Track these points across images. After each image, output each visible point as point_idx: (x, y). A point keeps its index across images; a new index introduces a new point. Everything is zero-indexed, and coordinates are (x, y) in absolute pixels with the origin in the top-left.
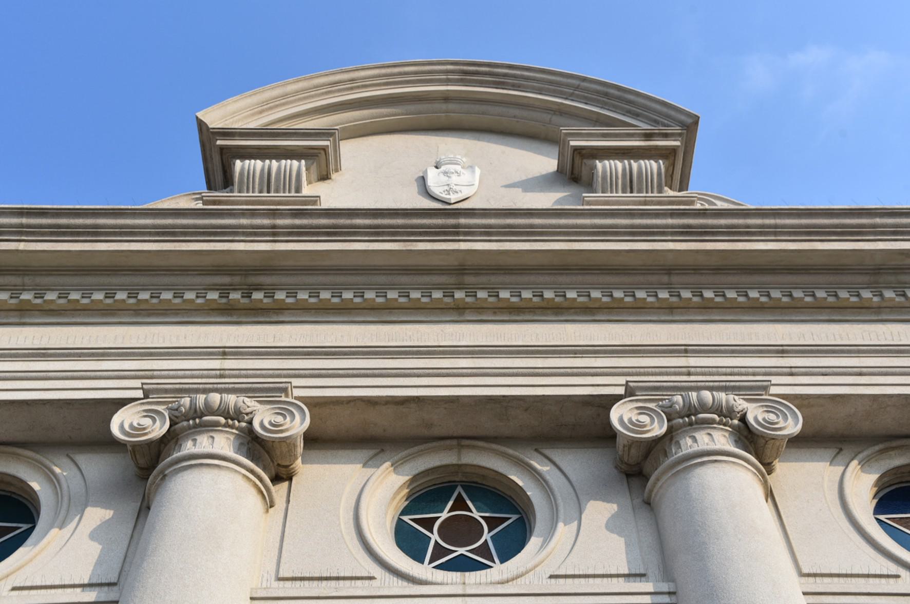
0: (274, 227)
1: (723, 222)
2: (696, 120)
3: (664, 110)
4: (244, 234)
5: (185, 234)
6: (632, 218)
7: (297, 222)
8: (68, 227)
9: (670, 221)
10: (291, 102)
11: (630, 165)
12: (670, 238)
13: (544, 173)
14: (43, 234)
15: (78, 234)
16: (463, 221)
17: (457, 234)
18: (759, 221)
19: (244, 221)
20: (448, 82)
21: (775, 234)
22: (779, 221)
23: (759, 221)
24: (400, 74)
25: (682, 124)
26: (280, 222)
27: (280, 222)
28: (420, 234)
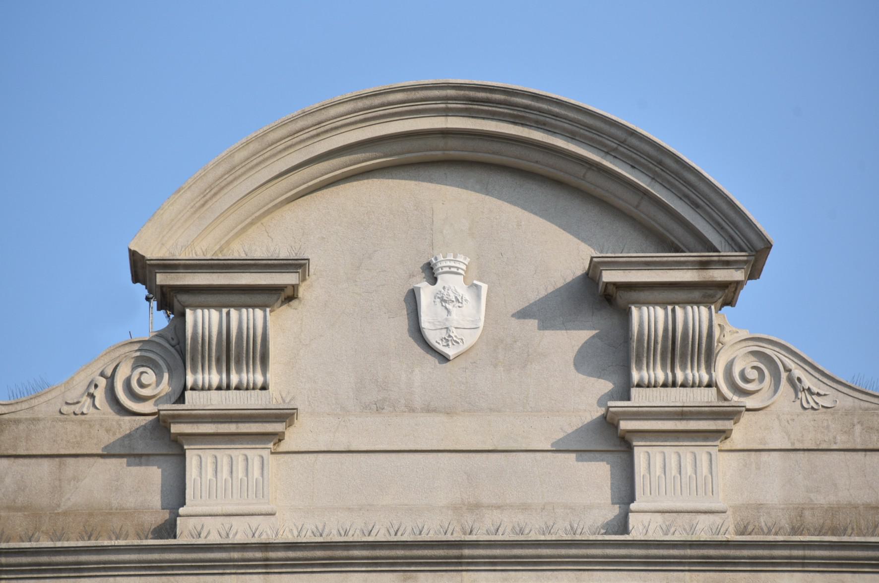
0: (267, 560)
1: (746, 552)
2: (768, 246)
3: (732, 214)
4: (234, 567)
5: (173, 568)
6: (647, 549)
7: (291, 554)
8: (49, 564)
9: (689, 552)
10: (240, 176)
11: (673, 311)
12: (687, 568)
13: (560, 284)
14: (23, 572)
15: (60, 571)
16: (466, 552)
17: (461, 564)
18: (786, 553)
19: (236, 555)
20: (446, 112)
21: (803, 565)
22: (808, 553)
23: (786, 553)
24: (383, 105)
25: (752, 248)
26: (272, 555)
27: (272, 555)
28: (421, 564)
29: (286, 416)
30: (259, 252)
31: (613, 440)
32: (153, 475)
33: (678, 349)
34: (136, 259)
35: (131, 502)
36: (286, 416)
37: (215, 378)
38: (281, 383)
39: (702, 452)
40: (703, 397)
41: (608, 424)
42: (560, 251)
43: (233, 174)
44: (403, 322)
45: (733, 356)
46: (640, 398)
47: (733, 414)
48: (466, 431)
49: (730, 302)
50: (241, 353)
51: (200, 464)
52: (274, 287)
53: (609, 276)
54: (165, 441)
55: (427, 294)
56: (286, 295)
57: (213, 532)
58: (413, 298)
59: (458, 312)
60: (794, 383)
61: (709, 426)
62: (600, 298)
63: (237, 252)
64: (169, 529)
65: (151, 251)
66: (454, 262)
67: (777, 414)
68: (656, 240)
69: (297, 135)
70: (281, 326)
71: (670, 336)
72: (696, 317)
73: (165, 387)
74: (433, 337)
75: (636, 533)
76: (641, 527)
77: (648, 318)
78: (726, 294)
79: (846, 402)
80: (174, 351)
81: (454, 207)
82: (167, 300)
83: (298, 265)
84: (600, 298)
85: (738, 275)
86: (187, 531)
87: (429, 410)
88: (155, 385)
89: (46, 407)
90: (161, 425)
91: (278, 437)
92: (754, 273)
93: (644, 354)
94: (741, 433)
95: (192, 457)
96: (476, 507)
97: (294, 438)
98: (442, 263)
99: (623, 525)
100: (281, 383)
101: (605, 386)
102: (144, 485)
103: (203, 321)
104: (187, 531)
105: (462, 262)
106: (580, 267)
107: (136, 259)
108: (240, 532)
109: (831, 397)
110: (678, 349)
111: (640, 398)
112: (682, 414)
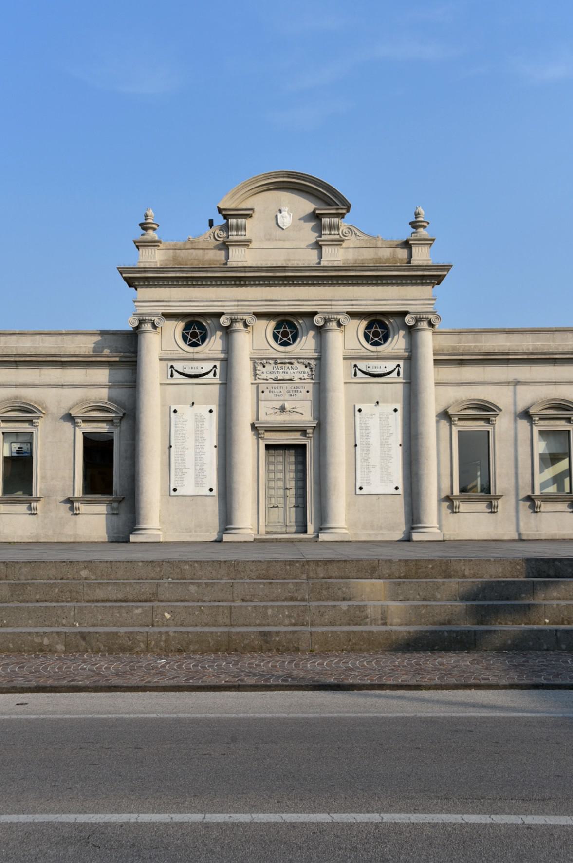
29: (250, 241)
30: (244, 207)
31: (318, 246)
32: (223, 252)
33: (332, 227)
34: (219, 209)
35: (218, 258)
36: (250, 241)
37: (235, 233)
38: (249, 234)
39: (337, 248)
40: (337, 237)
41: (317, 242)
42: (308, 206)
43: (238, 191)
44: (274, 221)
45: (343, 228)
46: (323, 237)
47: (343, 241)
48: (287, 244)
49: (343, 217)
50: (240, 228)
51: (415, 250)
52: (247, 215)
53: (317, 212)
54: (225, 246)
55: (279, 216)
56: (250, 216)
57: (420, 263)
58: (276, 217)
59: (286, 219)
60: (356, 234)
61: (338, 243)
62: (316, 217)
63: (240, 207)
64: (226, 264)
65: (222, 207)
66: (285, 210)
67: (351, 241)
68: (327, 203)
69: (251, 183)
70: (248, 222)
71: (237, 225)
72: (336, 220)
73: (225, 235)
74: (281, 225)
75: (322, 265)
76: (323, 264)
77: (326, 221)
78: (342, 216)
79: (366, 238)
80: (226, 228)
81: (286, 197)
82: (226, 217)
83: (252, 210)
84: (316, 217)
85: (344, 211)
86: (229, 264)
87: (280, 240)
88: (223, 234)
89: (201, 239)
90: (224, 243)
91: (248, 246)
92: (348, 211)
93: (324, 229)
94: (344, 245)
95: (324, 249)
96: (289, 260)
97: (252, 246)
98: (283, 209)
99: (319, 263)
100: (249, 234)
101: (317, 235)
102: (402, 254)
103: (233, 221)
104: (229, 264)
105: (287, 209)
106: (312, 210)
107: (219, 209)
108: (240, 264)
109: (363, 237)
110: (332, 227)
111: (323, 237)
112: (332, 241)
